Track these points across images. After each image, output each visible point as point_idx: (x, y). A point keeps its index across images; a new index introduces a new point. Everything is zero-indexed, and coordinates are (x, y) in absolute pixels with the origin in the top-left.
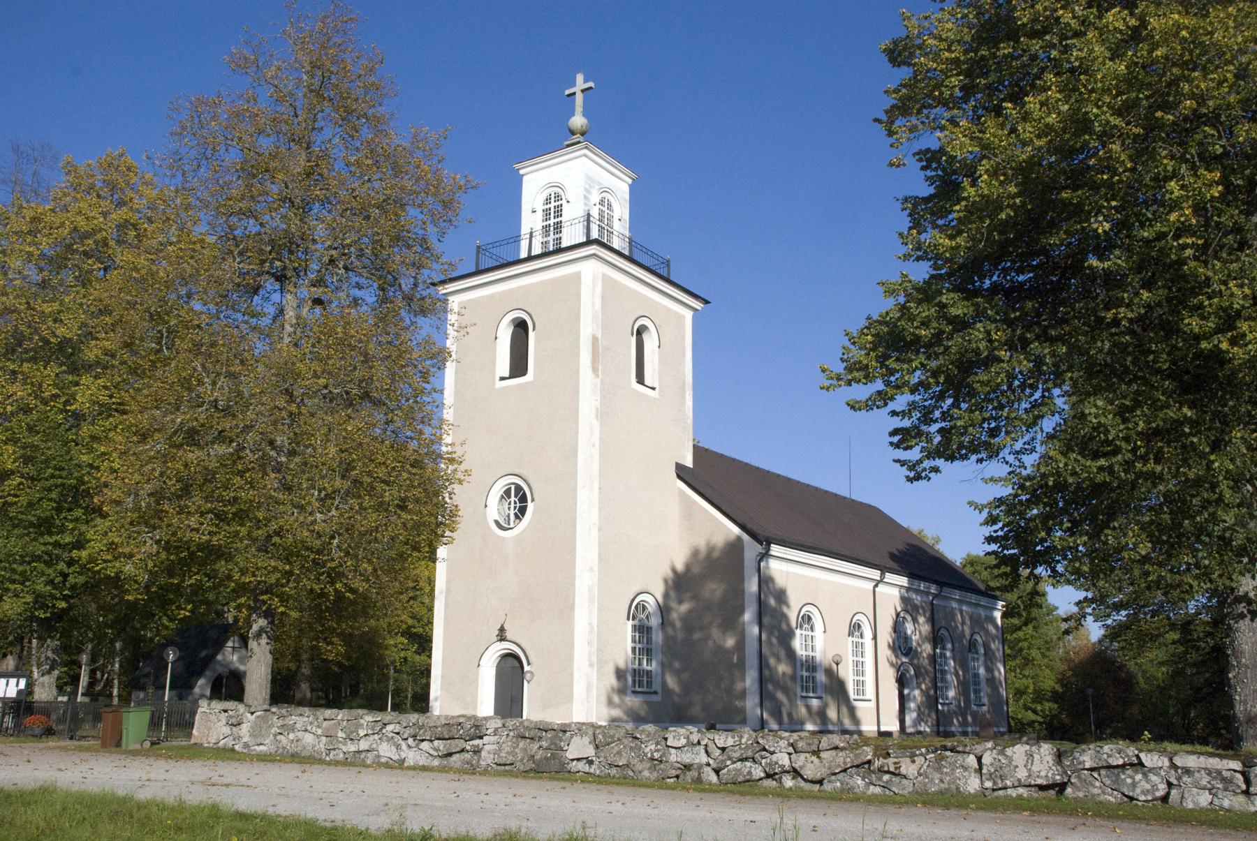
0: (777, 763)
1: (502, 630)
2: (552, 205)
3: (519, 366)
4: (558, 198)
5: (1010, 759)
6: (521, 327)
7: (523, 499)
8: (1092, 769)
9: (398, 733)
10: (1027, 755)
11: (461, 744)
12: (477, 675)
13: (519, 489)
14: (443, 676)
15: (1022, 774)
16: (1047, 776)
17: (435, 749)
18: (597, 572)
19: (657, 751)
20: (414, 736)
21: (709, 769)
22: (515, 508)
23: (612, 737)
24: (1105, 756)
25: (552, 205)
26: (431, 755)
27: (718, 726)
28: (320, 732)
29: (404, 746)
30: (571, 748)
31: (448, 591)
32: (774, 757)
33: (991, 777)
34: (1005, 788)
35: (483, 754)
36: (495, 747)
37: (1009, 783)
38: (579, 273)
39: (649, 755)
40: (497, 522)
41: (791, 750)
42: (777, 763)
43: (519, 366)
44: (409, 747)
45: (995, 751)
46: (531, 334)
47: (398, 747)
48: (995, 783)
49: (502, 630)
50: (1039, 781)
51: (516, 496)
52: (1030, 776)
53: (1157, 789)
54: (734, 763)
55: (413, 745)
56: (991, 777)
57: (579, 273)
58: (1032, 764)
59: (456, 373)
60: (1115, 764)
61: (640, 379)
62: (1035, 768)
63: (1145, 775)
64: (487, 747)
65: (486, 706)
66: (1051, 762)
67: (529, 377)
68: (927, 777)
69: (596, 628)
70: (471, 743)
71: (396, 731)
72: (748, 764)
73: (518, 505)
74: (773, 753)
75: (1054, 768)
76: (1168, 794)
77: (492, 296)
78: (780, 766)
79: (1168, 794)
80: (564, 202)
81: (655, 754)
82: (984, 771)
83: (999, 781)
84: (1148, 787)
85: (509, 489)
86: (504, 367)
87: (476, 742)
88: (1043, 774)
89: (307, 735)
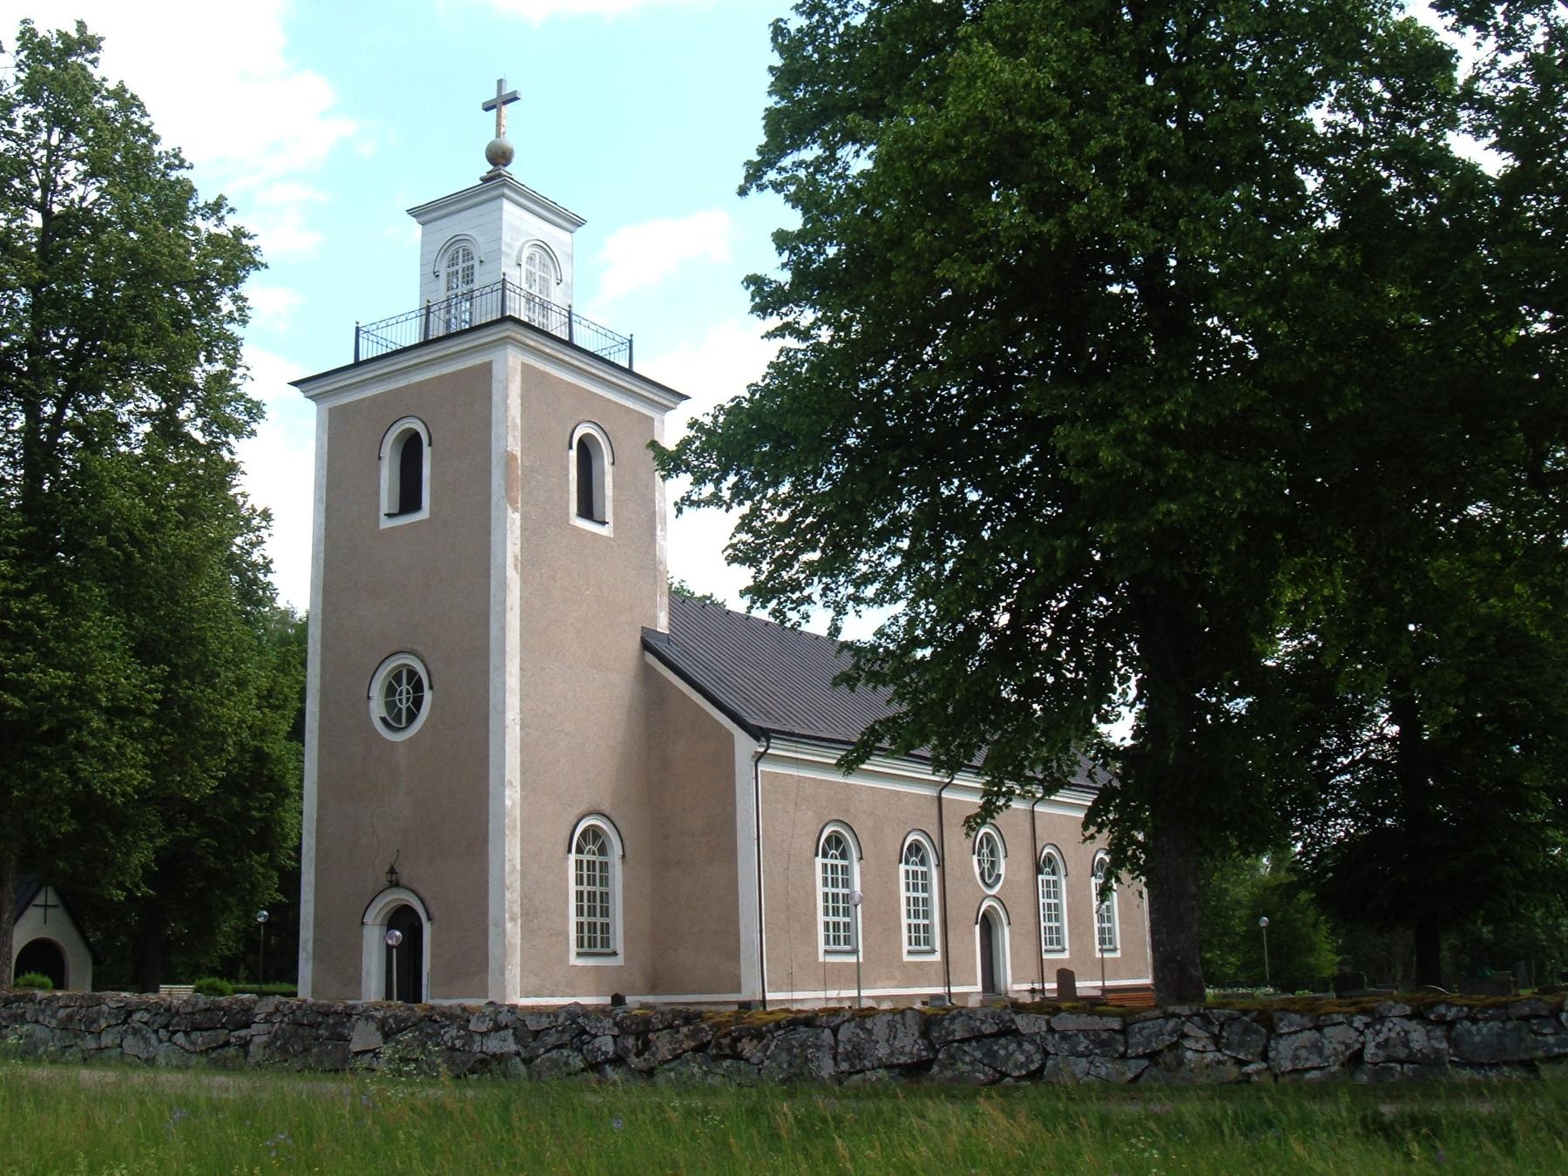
0: (599, 1049)
1: (392, 871)
2: (459, 267)
3: (409, 499)
4: (468, 255)
5: (870, 1032)
6: (411, 448)
7: (418, 687)
8: (962, 1041)
9: (146, 1023)
10: (889, 1025)
11: (222, 1035)
12: (361, 937)
13: (412, 673)
14: (316, 941)
15: (882, 1051)
16: (911, 1053)
17: (193, 1043)
18: (518, 789)
19: (459, 1037)
20: (166, 1027)
21: (518, 1059)
22: (408, 699)
23: (404, 1020)
24: (978, 1023)
25: (459, 267)
26: (187, 1051)
27: (736, 1008)
28: (54, 1023)
29: (153, 1038)
30: (355, 1036)
31: (320, 820)
32: (597, 1043)
33: (847, 1058)
34: (862, 1071)
35: (252, 1048)
36: (265, 1038)
37: (868, 1064)
38: (490, 363)
39: (450, 1044)
40: (383, 720)
41: (616, 1031)
42: (599, 1049)
43: (409, 499)
44: (160, 1041)
45: (853, 1023)
46: (427, 452)
47: (146, 1041)
48: (852, 1066)
49: (392, 871)
50: (903, 1060)
51: (408, 684)
52: (892, 1054)
53: (1032, 1061)
54: (547, 1051)
55: (165, 1039)
56: (847, 1058)
57: (490, 363)
58: (895, 1037)
59: (327, 511)
60: (987, 1032)
61: (587, 509)
62: (897, 1043)
63: (1020, 1045)
64: (257, 1040)
65: (372, 987)
66: (917, 1034)
67: (424, 514)
68: (775, 1060)
69: (518, 867)
70: (236, 1033)
71: (144, 1020)
72: (565, 1052)
73: (397, 697)
74: (595, 1036)
75: (920, 1041)
76: (1042, 1067)
77: (374, 399)
78: (603, 1053)
79: (1042, 1067)
80: (476, 263)
81: (457, 1042)
82: (841, 1050)
83: (857, 1061)
84: (1022, 1058)
85: (400, 673)
86: (387, 495)
87: (243, 1033)
88: (907, 1049)
89: (38, 1028)
